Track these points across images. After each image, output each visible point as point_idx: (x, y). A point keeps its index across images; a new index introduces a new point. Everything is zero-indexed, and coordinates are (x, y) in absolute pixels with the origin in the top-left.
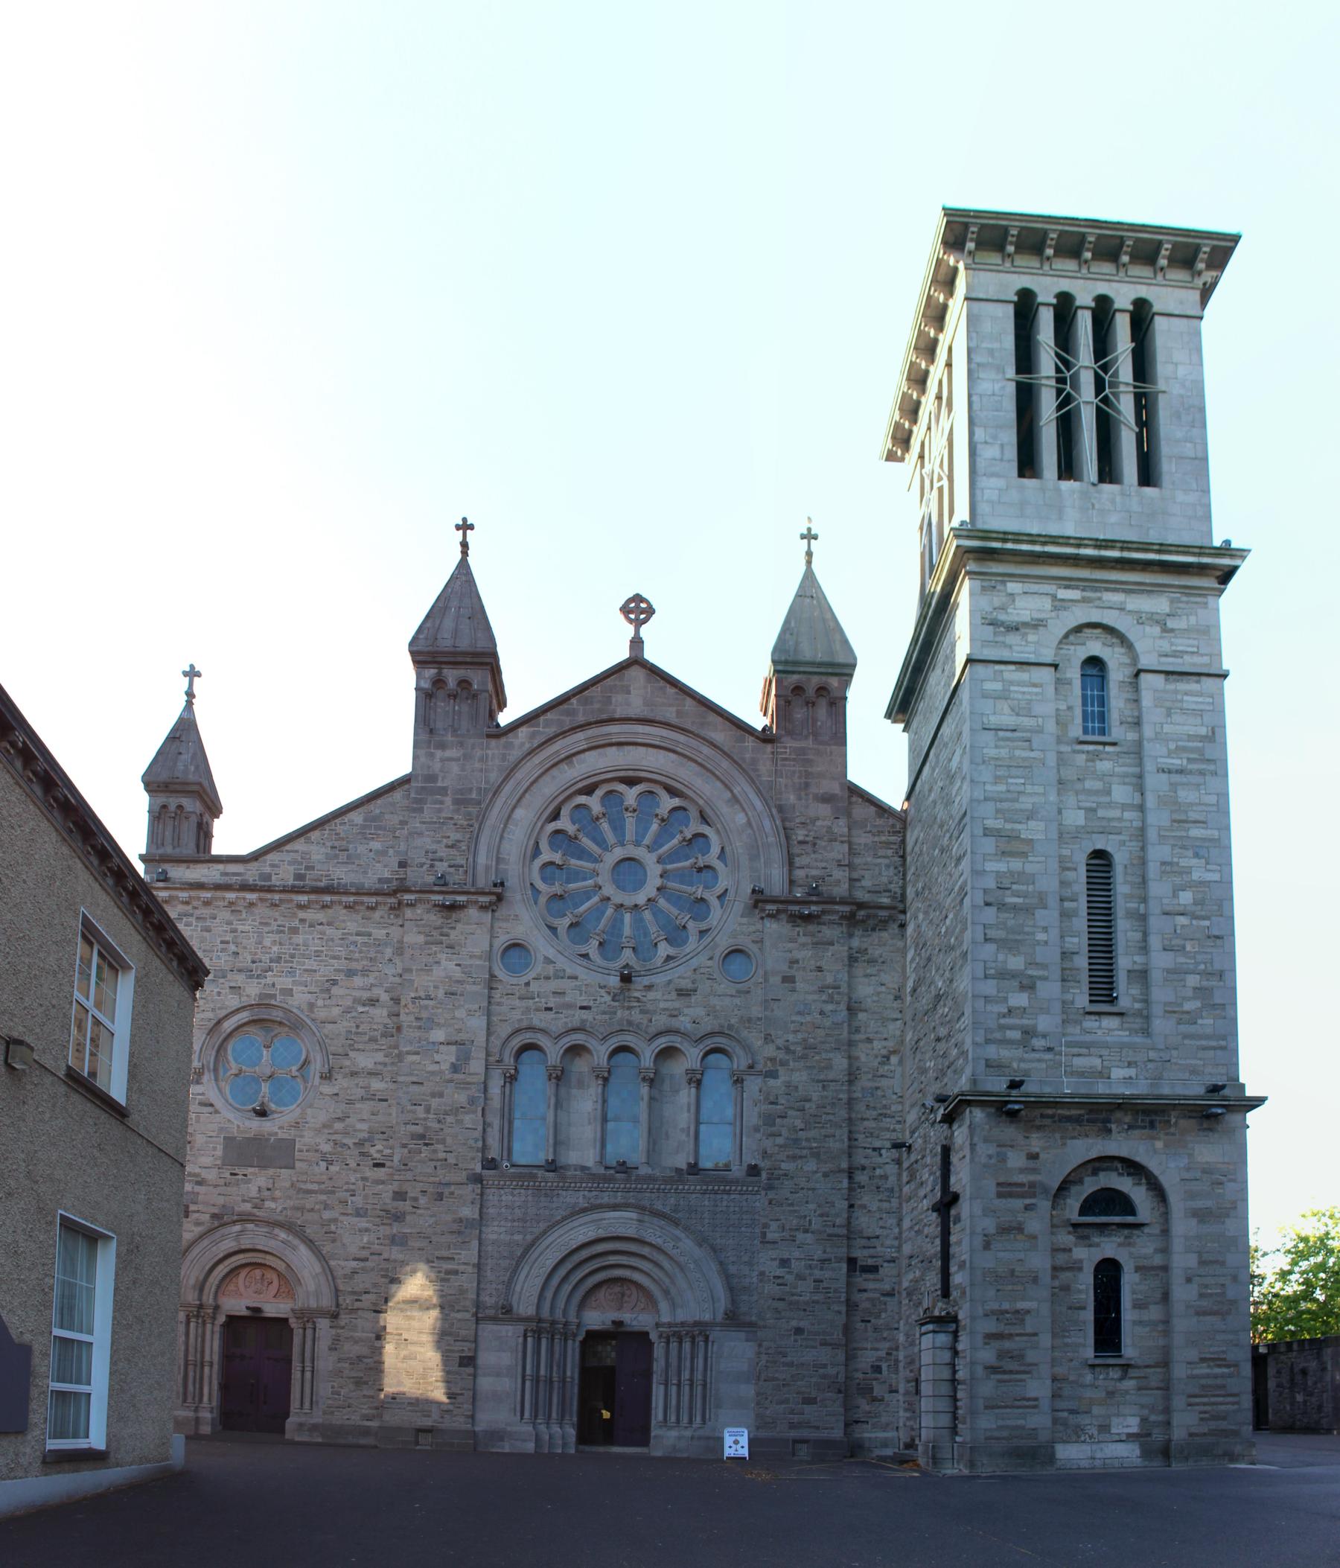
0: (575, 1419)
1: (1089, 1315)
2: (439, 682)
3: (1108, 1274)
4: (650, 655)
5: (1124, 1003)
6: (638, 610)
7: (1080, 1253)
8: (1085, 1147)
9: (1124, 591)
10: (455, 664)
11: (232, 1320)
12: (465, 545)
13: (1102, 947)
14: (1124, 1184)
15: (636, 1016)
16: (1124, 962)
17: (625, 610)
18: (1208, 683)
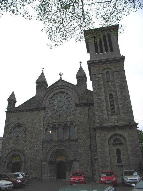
0: (56, 175)
1: (116, 157)
2: (39, 86)
3: (118, 151)
4: (62, 79)
5: (116, 112)
6: (61, 74)
7: (114, 148)
8: (112, 133)
9: (105, 64)
10: (40, 83)
11: (13, 163)
12: (43, 70)
13: (112, 105)
14: (119, 137)
15: (61, 120)
16: (116, 107)
17: (59, 74)
18: (122, 72)
